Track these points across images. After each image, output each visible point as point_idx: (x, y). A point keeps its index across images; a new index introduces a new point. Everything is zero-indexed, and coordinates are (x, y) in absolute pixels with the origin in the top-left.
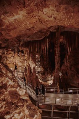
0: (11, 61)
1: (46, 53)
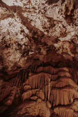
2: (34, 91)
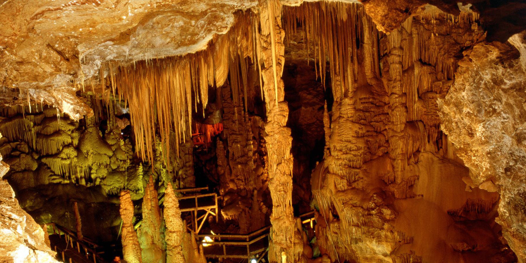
0: (66, 171)
1: (412, 53)
2: (14, 145)
